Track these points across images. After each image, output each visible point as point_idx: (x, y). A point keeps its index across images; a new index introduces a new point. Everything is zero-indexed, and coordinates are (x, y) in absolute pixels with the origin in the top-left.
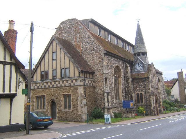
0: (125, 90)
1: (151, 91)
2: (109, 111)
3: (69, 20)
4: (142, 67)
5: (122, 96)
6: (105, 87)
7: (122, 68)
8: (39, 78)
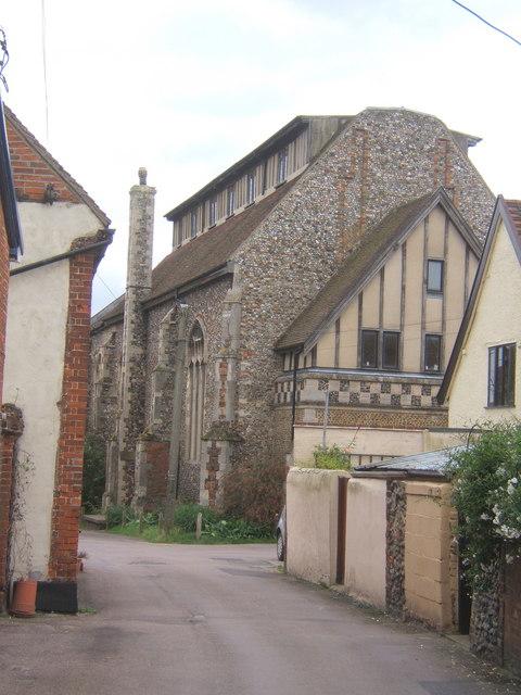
8: (350, 356)
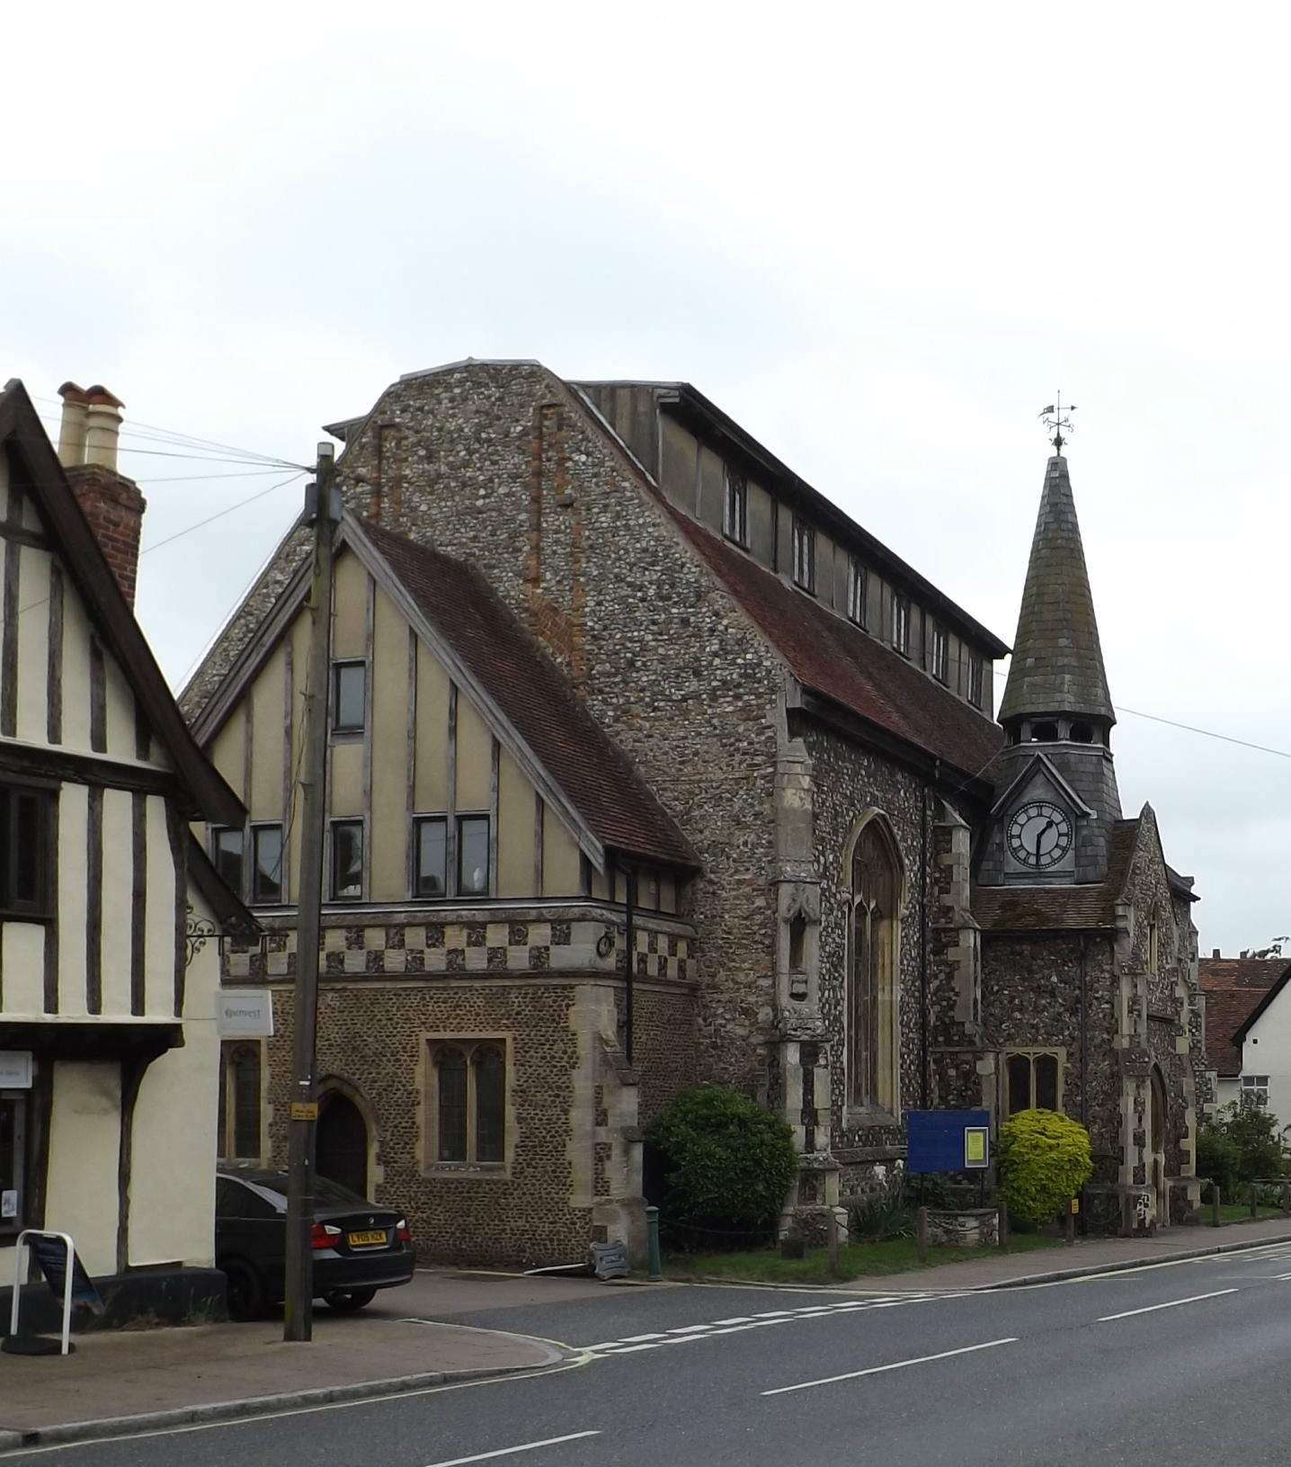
0: (923, 1025)
1: (1125, 1043)
2: (814, 1188)
3: (477, 375)
4: (1064, 841)
5: (898, 1072)
6: (785, 1000)
7: (906, 840)
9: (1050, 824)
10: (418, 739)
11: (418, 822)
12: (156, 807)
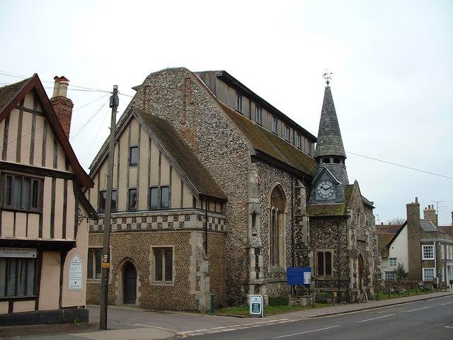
0: (293, 243)
2: (259, 290)
6: (250, 235)
7: (287, 192)
9: (322, 187)
10: (150, 167)
11: (151, 188)
12: (70, 183)
